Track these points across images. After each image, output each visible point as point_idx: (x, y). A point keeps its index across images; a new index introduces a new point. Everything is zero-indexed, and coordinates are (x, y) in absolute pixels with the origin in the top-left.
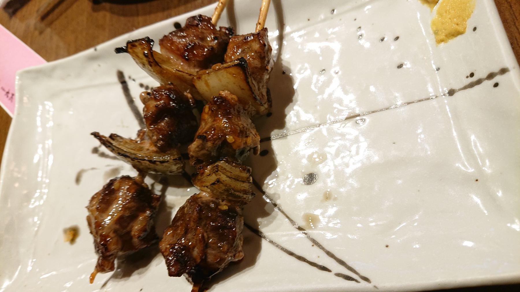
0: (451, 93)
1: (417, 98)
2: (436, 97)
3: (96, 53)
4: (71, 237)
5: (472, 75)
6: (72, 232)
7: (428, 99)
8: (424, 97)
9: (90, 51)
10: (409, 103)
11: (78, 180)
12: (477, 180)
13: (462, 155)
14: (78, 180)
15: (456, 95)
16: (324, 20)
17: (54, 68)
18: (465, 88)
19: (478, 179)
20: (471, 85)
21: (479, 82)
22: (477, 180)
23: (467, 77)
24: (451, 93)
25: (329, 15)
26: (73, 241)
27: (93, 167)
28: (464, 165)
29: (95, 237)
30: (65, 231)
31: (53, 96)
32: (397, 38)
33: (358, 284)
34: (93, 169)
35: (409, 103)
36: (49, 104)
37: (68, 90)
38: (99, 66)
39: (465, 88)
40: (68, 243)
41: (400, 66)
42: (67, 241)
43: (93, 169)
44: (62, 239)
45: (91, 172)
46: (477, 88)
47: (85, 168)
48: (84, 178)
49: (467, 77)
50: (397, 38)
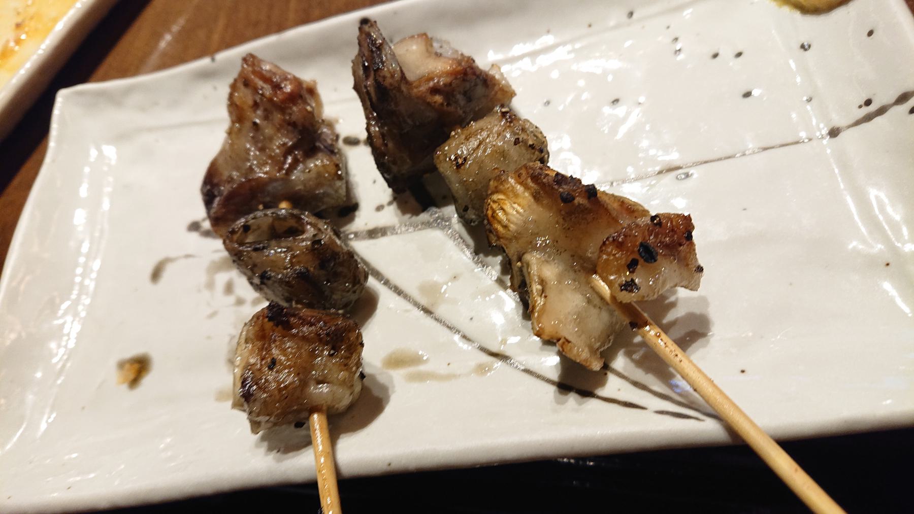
0: (834, 133)
1: (779, 142)
2: (810, 140)
3: (214, 65)
4: (132, 376)
5: (868, 103)
6: (136, 366)
7: (797, 143)
8: (789, 140)
9: (205, 62)
10: (765, 149)
11: (156, 275)
12: (888, 264)
13: (860, 224)
14: (156, 275)
15: (841, 135)
16: (617, 27)
17: (129, 90)
18: (858, 123)
19: (890, 261)
20: (868, 118)
21: (882, 111)
22: (888, 264)
23: (860, 107)
24: (834, 133)
25: (624, 18)
26: (134, 382)
27: (189, 252)
28: (864, 241)
29: (233, 122)
30: (121, 365)
31: (120, 138)
32: (739, 55)
33: (702, 423)
34: (188, 256)
35: (765, 149)
36: (110, 151)
37: (150, 130)
38: (215, 88)
39: (858, 123)
40: (124, 387)
41: (747, 95)
42: (124, 383)
43: (188, 256)
44: (111, 376)
45: (183, 262)
46: (878, 120)
47: (172, 255)
48: (169, 273)
49: (860, 107)
50: (739, 55)
